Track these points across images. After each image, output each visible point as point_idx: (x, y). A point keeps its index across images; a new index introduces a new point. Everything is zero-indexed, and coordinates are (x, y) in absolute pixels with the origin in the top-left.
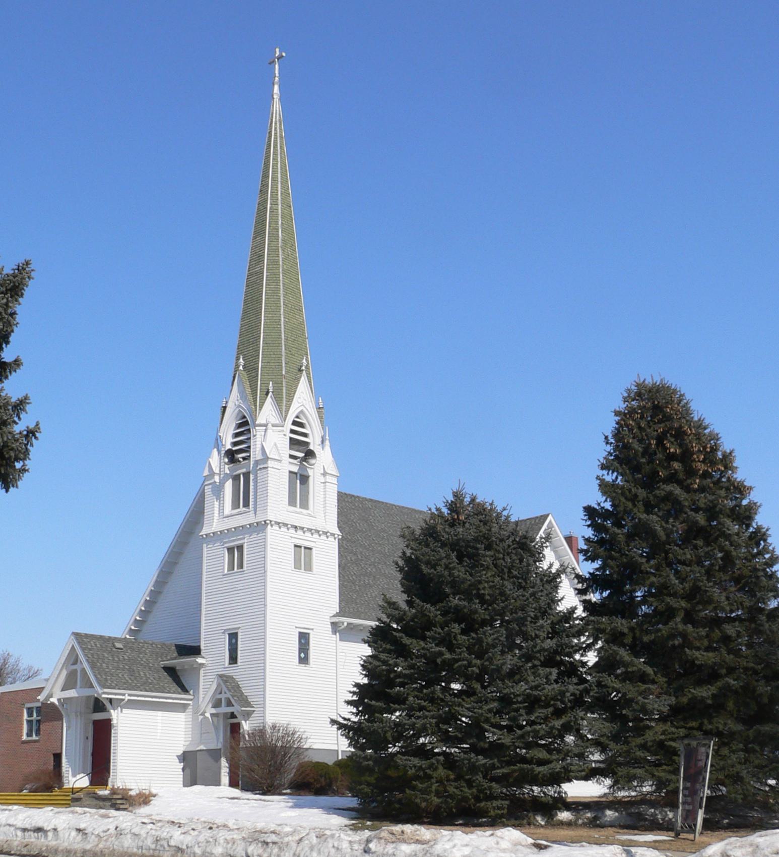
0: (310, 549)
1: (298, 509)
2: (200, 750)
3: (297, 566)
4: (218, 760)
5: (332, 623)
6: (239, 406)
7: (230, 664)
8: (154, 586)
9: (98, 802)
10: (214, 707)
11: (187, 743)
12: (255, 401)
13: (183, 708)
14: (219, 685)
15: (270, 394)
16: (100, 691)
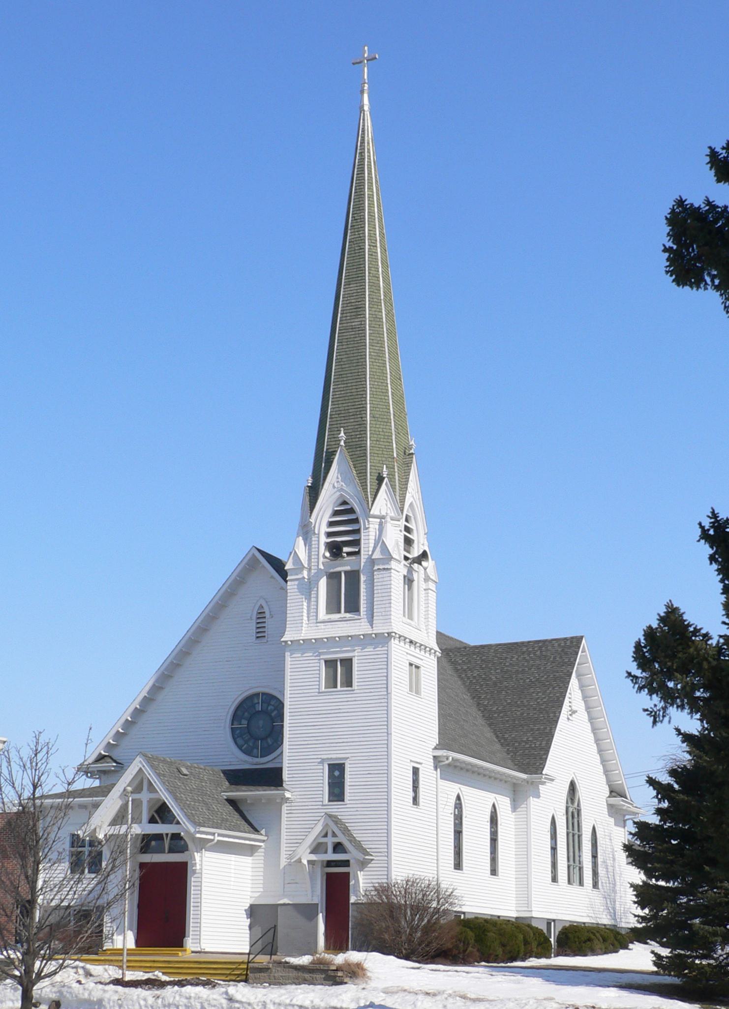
0: (417, 667)
1: (343, 614)
2: (284, 905)
3: (332, 683)
4: (313, 917)
5: (434, 757)
6: (342, 490)
7: (329, 801)
8: (148, 693)
9: (300, 974)
10: (313, 852)
11: (257, 895)
12: (365, 489)
13: (251, 850)
14: (326, 826)
15: (386, 480)
16: (192, 830)
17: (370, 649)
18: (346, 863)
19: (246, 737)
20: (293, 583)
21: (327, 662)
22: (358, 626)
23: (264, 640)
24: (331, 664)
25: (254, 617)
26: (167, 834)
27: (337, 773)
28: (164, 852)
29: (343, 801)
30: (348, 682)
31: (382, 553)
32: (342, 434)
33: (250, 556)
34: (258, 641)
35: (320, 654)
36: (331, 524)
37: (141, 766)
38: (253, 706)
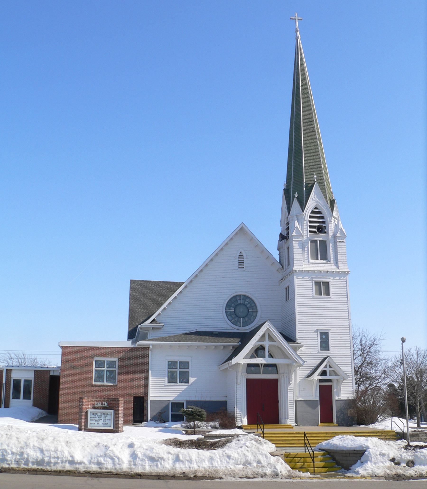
2: (301, 401)
6: (317, 201)
17: (337, 278)
18: (330, 381)
19: (234, 316)
20: (296, 242)
21: (316, 282)
22: (330, 267)
23: (243, 269)
24: (318, 284)
25: (238, 257)
26: (262, 364)
27: (324, 337)
28: (260, 374)
29: (329, 350)
30: (328, 293)
31: (340, 234)
32: (315, 176)
33: (240, 227)
34: (240, 269)
35: (312, 278)
36: (311, 217)
37: (268, 327)
38: (237, 301)
